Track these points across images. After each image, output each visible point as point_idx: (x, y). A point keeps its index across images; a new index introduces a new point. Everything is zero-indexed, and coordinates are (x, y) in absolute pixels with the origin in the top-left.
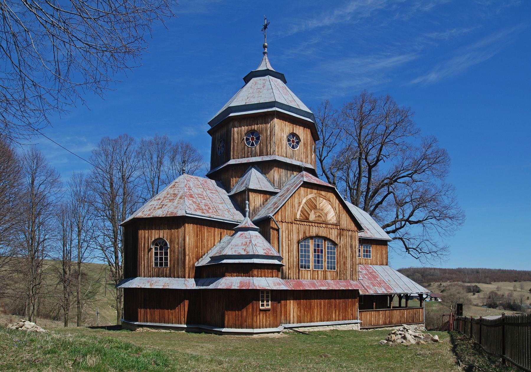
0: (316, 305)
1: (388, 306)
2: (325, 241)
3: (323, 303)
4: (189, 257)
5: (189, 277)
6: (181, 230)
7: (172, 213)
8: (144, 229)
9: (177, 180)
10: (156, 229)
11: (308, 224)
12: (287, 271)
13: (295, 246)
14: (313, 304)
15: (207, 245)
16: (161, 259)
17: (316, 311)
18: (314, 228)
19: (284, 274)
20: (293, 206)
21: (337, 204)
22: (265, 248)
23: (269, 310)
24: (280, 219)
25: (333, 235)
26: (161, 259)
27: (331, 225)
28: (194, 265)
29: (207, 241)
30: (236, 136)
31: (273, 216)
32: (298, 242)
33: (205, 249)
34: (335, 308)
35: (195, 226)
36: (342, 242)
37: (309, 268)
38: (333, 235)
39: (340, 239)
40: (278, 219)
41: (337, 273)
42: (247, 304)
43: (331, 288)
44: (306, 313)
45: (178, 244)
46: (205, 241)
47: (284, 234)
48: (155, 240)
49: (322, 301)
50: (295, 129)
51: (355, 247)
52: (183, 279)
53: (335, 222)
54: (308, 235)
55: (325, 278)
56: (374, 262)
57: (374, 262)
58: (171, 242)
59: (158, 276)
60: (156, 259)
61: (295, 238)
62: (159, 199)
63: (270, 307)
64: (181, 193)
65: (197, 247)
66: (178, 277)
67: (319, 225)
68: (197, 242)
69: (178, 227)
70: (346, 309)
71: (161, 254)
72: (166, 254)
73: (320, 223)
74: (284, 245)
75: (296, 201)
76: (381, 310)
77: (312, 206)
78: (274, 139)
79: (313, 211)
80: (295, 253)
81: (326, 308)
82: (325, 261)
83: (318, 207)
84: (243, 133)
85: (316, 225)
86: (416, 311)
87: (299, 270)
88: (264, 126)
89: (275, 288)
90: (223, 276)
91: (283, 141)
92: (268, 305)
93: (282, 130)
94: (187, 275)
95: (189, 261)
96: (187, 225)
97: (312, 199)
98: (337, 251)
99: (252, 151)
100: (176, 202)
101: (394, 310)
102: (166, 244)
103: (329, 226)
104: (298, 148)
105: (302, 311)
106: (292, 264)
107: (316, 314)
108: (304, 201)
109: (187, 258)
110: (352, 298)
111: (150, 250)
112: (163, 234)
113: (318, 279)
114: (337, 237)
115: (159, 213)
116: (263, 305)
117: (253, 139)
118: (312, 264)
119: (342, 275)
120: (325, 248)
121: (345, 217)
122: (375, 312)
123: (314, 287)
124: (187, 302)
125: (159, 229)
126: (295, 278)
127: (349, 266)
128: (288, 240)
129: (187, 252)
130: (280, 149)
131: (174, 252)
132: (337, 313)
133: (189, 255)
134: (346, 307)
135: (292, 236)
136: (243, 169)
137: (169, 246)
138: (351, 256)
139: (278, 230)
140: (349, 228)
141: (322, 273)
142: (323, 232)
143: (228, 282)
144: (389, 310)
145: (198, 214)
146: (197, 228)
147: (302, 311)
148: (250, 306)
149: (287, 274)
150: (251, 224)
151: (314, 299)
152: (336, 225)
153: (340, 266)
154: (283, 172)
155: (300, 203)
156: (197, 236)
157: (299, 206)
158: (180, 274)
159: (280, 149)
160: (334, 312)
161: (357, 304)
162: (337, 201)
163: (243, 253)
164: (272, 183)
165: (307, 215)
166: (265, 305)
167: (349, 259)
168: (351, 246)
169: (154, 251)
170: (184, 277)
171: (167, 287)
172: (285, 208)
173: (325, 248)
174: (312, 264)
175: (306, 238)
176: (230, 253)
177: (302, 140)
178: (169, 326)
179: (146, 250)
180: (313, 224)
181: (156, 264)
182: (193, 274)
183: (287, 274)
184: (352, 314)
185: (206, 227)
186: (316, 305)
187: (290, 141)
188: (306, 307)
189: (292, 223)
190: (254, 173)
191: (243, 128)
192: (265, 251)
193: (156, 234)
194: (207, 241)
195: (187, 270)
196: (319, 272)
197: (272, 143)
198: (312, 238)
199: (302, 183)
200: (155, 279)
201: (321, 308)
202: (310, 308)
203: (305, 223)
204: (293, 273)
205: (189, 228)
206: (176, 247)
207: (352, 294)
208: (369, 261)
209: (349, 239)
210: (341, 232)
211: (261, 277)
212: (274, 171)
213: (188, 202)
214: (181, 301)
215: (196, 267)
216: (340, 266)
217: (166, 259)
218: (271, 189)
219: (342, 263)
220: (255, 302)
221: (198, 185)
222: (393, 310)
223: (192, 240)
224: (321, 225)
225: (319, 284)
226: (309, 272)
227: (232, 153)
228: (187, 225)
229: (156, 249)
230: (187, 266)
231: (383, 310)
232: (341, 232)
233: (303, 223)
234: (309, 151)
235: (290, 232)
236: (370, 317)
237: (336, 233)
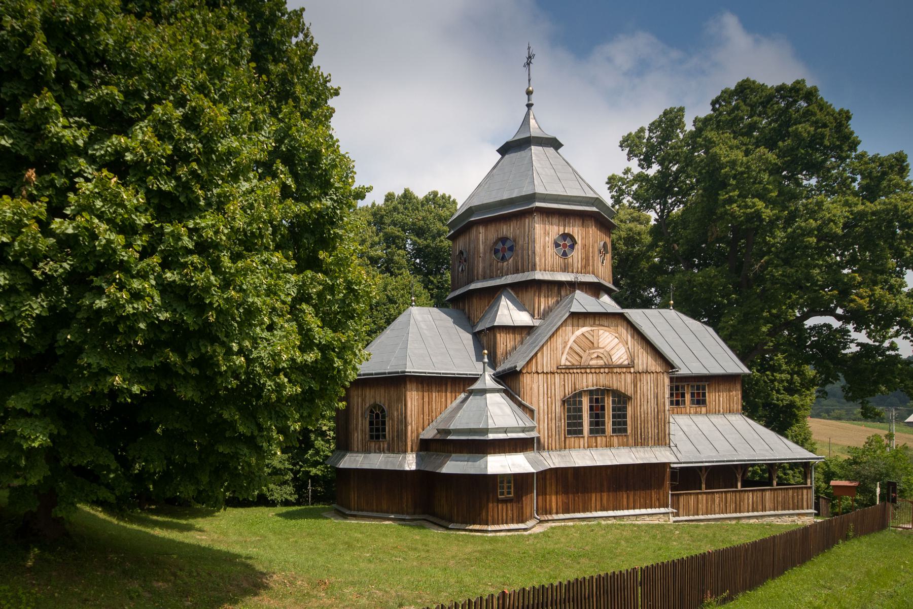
1: (809, 485)
12: (546, 440)
18: (590, 375)
24: (534, 370)
25: (623, 383)
27: (626, 368)
53: (626, 363)
67: (597, 371)
71: (377, 423)
76: (717, 492)
83: (596, 345)
85: (593, 371)
92: (509, 493)
93: (546, 233)
101: (745, 491)
103: (615, 370)
109: (409, 428)
116: (502, 494)
122: (705, 496)
128: (548, 398)
135: (553, 391)
136: (492, 294)
138: (656, 410)
142: (604, 381)
144: (733, 491)
152: (627, 367)
155: (566, 343)
166: (506, 493)
177: (579, 242)
178: (607, 461)
180: (588, 371)
184: (659, 500)
187: (560, 245)
189: (553, 373)
199: (567, 315)
215: (421, 440)
231: (722, 492)
236: (696, 503)
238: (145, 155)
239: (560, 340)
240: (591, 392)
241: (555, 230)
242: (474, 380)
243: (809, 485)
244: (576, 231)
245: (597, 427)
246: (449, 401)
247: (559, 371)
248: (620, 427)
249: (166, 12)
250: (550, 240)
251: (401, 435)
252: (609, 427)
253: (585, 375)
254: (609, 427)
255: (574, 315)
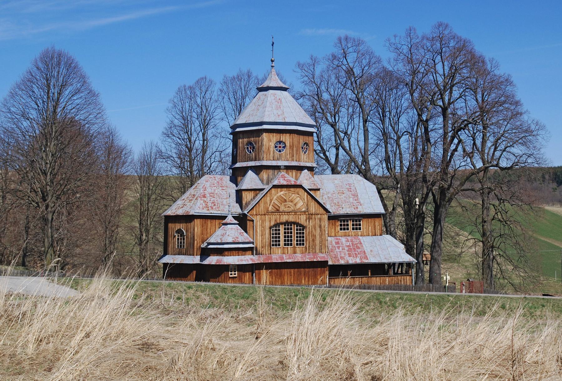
0: (286, 273)
1: (410, 274)
2: (294, 225)
3: (279, 272)
4: (197, 242)
5: (197, 255)
6: (192, 223)
7: (187, 212)
8: (172, 223)
9: (199, 182)
10: (178, 223)
11: (279, 214)
13: (267, 231)
14: (283, 272)
15: (210, 232)
16: (181, 242)
17: (286, 278)
19: (258, 251)
20: (265, 203)
21: (305, 196)
22: (234, 237)
23: (236, 277)
24: (255, 213)
25: (302, 219)
26: (181, 242)
28: (200, 246)
29: (210, 229)
30: (241, 145)
31: (248, 213)
32: (270, 228)
33: (209, 235)
34: (304, 275)
35: (202, 220)
36: (311, 224)
37: (279, 245)
38: (302, 220)
39: (309, 222)
40: (253, 213)
41: (306, 248)
42: (222, 274)
43: (296, 261)
44: (277, 279)
45: (190, 233)
46: (209, 229)
47: (258, 223)
48: (178, 230)
49: (292, 270)
50: (282, 137)
51: (325, 227)
52: (193, 256)
54: (278, 222)
55: (295, 252)
56: (365, 234)
57: (365, 234)
58: (186, 231)
59: (179, 254)
60: (178, 242)
61: (267, 225)
62: (184, 200)
63: (236, 275)
64: (198, 194)
65: (202, 234)
66: (190, 255)
67: (288, 214)
68: (202, 231)
69: (190, 222)
70: (315, 276)
71: (181, 239)
72: (184, 239)
73: (289, 212)
74: (258, 231)
75: (268, 199)
77: (281, 201)
78: (264, 148)
79: (283, 204)
80: (267, 235)
81: (296, 275)
82: (294, 240)
84: (245, 143)
85: (286, 213)
86: (401, 278)
87: (271, 248)
88: (257, 138)
89: (237, 263)
90: (209, 256)
91: (270, 149)
92: (235, 274)
93: (270, 141)
94: (195, 254)
95: (197, 244)
96: (196, 220)
97: (282, 195)
98: (306, 231)
99: (250, 157)
100: (193, 202)
102: (183, 233)
104: (285, 151)
105: (274, 278)
106: (265, 243)
107: (286, 280)
108: (275, 198)
109: (196, 242)
110: (321, 268)
111: (175, 236)
112: (181, 226)
113: (288, 253)
114: (306, 220)
115: (180, 212)
116: (231, 274)
117: (251, 148)
118: (282, 243)
119: (311, 249)
120: (294, 230)
121: (313, 204)
123: (281, 260)
124: (195, 272)
125: (180, 223)
126: (267, 254)
127: (317, 242)
129: (196, 238)
130: (268, 155)
131: (188, 238)
132: (307, 279)
133: (197, 240)
134: (316, 274)
136: (244, 171)
137: (185, 234)
139: (253, 221)
140: (318, 212)
141: (292, 249)
142: (291, 218)
143: (211, 260)
145: (205, 212)
146: (203, 221)
147: (274, 278)
148: (223, 275)
149: (261, 251)
150: (231, 220)
151: (285, 268)
153: (309, 243)
154: (271, 172)
155: (271, 200)
156: (203, 227)
157: (271, 202)
158: (191, 253)
159: (268, 155)
160: (303, 278)
161: (327, 273)
162: (306, 193)
163: (219, 241)
164: (262, 181)
165: (277, 207)
167: (318, 237)
168: (320, 227)
169: (177, 237)
170: (194, 255)
171: (182, 262)
172: (259, 205)
173: (294, 230)
174: (282, 243)
175: (277, 225)
176: (212, 242)
179: (173, 237)
180: (283, 214)
181: (178, 246)
182: (199, 253)
183: (261, 251)
185: (209, 220)
186: (286, 273)
188: (277, 275)
189: (265, 215)
190: (250, 173)
191: (245, 139)
192: (234, 240)
193: (178, 226)
194: (210, 229)
195: (195, 250)
196: (289, 249)
197: (262, 152)
198: (282, 223)
200: (177, 256)
201: (291, 275)
202: (281, 276)
203: (276, 214)
204: (266, 251)
205: (197, 222)
206: (190, 234)
207: (323, 264)
208: (360, 233)
209: (318, 221)
210: (310, 216)
211: (230, 256)
212: (264, 173)
213: (200, 202)
214: (191, 271)
215: (202, 248)
216: (309, 243)
217: (184, 242)
218: (260, 186)
219: (311, 240)
220: (225, 272)
221: (214, 184)
222: (371, 277)
223: (199, 229)
224: (291, 213)
225: (287, 257)
226: (280, 250)
227: (238, 158)
228: (196, 220)
229: (178, 236)
230: (195, 248)
232: (310, 216)
233: (274, 214)
234: (295, 151)
235: (263, 221)
237: (305, 218)
238: (430, 182)
239: (268, 199)
240: (284, 224)
241: (275, 138)
242: (224, 217)
243: (410, 274)
244: (286, 138)
245: (288, 242)
246: (217, 228)
247: (268, 214)
248: (301, 242)
249: (442, 266)
250: (272, 145)
251: (191, 244)
252: (294, 239)
253: (282, 216)
254: (294, 239)
255: (275, 187)
